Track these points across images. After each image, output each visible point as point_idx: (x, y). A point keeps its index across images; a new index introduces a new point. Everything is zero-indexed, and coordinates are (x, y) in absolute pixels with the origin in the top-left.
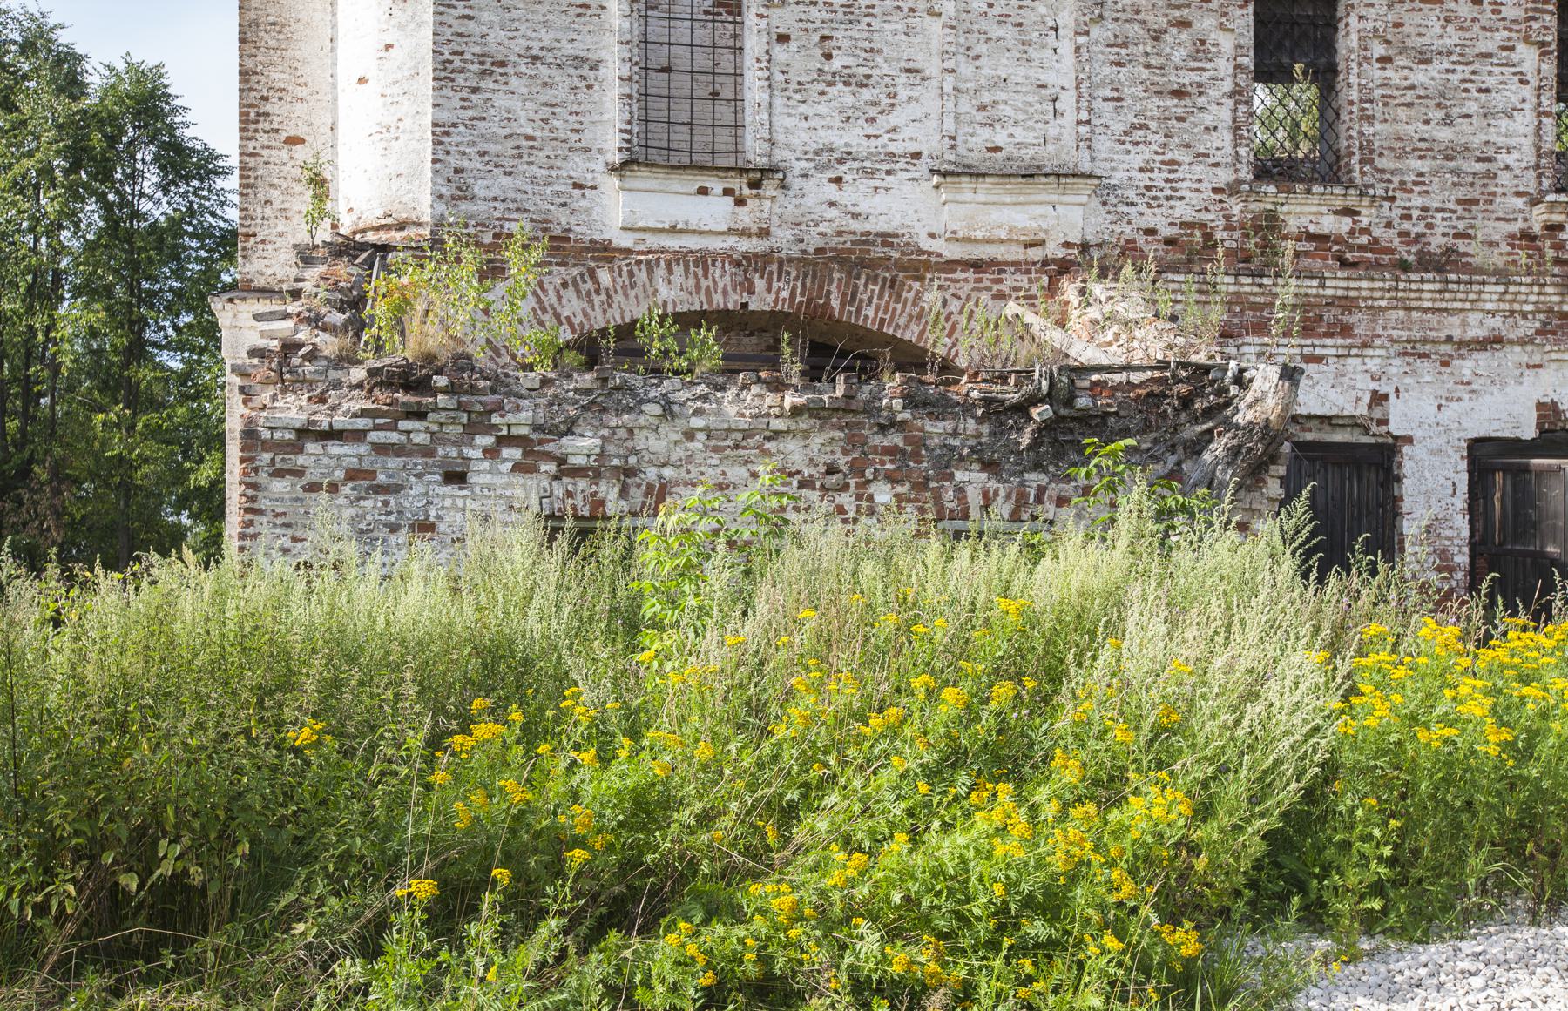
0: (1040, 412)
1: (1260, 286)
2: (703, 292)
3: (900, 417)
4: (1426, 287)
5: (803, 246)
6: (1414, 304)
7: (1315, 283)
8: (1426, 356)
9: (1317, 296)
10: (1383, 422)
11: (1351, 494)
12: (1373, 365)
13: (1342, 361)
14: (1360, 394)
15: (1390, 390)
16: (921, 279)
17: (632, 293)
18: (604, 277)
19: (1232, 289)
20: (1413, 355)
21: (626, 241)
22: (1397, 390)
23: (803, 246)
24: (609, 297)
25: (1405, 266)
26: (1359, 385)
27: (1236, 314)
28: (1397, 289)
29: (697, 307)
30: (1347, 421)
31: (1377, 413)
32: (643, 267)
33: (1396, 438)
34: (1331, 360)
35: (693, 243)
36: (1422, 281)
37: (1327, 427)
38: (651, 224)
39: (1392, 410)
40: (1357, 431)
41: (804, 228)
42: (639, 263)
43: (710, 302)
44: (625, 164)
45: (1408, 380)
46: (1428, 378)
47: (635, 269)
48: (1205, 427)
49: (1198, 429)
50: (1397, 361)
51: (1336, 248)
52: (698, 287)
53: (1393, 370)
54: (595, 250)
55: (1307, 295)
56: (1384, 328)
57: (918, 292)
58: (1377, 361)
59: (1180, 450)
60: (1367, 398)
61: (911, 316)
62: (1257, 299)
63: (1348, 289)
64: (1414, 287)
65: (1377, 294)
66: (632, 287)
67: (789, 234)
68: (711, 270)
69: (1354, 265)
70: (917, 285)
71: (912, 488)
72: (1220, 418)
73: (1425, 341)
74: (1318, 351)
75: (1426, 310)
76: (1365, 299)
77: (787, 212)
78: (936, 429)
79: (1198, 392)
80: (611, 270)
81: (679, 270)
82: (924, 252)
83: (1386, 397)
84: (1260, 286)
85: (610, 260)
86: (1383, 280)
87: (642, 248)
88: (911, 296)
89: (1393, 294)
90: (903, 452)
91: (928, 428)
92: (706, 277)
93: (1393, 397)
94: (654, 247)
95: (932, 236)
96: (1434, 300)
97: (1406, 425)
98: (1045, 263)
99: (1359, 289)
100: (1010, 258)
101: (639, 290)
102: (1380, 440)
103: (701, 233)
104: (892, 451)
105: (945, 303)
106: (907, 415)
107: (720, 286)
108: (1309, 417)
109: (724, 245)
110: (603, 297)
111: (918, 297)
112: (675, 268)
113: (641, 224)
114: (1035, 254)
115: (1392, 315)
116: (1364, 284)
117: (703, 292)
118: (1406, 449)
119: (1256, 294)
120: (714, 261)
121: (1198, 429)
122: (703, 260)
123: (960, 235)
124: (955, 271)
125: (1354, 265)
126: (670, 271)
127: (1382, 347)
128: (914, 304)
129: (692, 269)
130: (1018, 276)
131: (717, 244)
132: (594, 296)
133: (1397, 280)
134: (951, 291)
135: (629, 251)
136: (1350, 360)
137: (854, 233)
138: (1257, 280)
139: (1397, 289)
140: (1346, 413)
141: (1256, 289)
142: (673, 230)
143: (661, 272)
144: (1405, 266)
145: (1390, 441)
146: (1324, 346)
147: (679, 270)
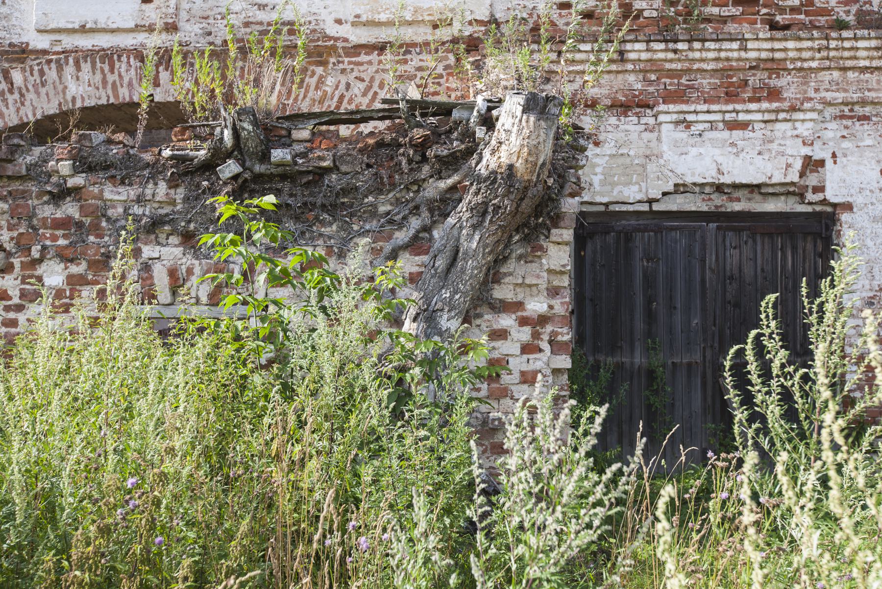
0: (230, 168)
1: (675, 51)
2: (109, 86)
3: (71, 183)
4: (861, 44)
5: (210, 39)
6: (849, 64)
7: (735, 45)
8: (865, 118)
9: (739, 59)
10: (819, 189)
11: (784, 267)
12: (804, 129)
13: (769, 126)
14: (790, 160)
15: (826, 155)
16: (324, 64)
17: (43, 91)
18: (17, 77)
19: (644, 56)
20: (851, 117)
21: (41, 42)
22: (834, 155)
23: (210, 39)
24: (22, 95)
25: (841, 25)
26: (789, 151)
27: (651, 83)
28: (828, 48)
29: (104, 101)
30: (778, 190)
31: (812, 180)
32: (53, 65)
33: (835, 205)
34: (757, 126)
35: (104, 41)
36: (856, 38)
37: (758, 197)
38: (62, 25)
39: (828, 176)
40: (792, 200)
41: (211, 21)
42: (49, 62)
43: (116, 96)
44: (611, 106)
45: (846, 144)
46: (869, 142)
47: (46, 68)
48: (450, 182)
49: (443, 185)
50: (833, 125)
51: (764, 11)
52: (104, 82)
53: (829, 134)
54: (13, 53)
55: (728, 59)
56: (817, 90)
57: (321, 77)
58: (810, 125)
59: (425, 214)
60: (798, 165)
61: (314, 100)
62: (673, 66)
63: (772, 50)
64: (847, 44)
65: (806, 55)
66: (43, 85)
67: (197, 28)
68: (117, 66)
69: (786, 27)
70: (320, 70)
71: (89, 267)
72: (465, 168)
73: (863, 103)
74: (742, 117)
75: (864, 70)
76: (793, 60)
77: (195, 7)
78: (116, 195)
79: (437, 136)
80: (23, 70)
81: (86, 67)
82: (330, 38)
83: (821, 163)
84: (675, 51)
85: (22, 61)
86: (811, 39)
87: (58, 49)
88: (314, 80)
89: (824, 53)
90: (79, 225)
91: (107, 195)
92: (112, 71)
93: (829, 163)
94: (69, 47)
95: (339, 22)
96: (872, 58)
97: (844, 191)
98: (455, 41)
99: (785, 50)
100: (419, 40)
101: (49, 88)
102: (818, 208)
103: (113, 31)
104: (64, 224)
105: (348, 86)
106: (78, 180)
107: (126, 80)
108: (736, 186)
109: (134, 42)
110: (16, 96)
111: (321, 81)
112: (83, 65)
113: (53, 26)
114: (444, 34)
115: (826, 76)
116: (791, 44)
117: (109, 86)
118: (845, 217)
119: (671, 61)
120: (119, 57)
121: (443, 185)
122: (109, 56)
123: (364, 18)
124: (359, 55)
125: (786, 27)
126: (78, 68)
127: (813, 110)
128: (317, 88)
129: (99, 65)
130: (424, 56)
131: (128, 41)
132: (8, 95)
133: (827, 38)
134: (355, 74)
135: (45, 52)
136: (778, 126)
137: (261, 23)
138: (671, 45)
139: (828, 48)
140: (774, 180)
141: (670, 55)
142: (83, 30)
143: (69, 69)
144: (841, 25)
145: (829, 209)
146: (748, 112)
147: (86, 67)
